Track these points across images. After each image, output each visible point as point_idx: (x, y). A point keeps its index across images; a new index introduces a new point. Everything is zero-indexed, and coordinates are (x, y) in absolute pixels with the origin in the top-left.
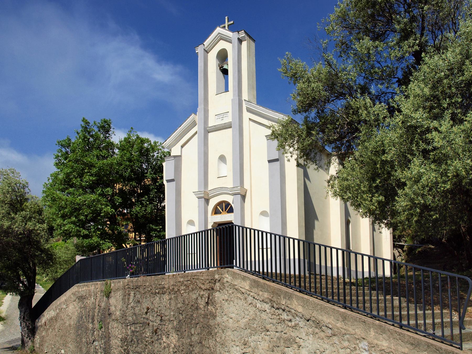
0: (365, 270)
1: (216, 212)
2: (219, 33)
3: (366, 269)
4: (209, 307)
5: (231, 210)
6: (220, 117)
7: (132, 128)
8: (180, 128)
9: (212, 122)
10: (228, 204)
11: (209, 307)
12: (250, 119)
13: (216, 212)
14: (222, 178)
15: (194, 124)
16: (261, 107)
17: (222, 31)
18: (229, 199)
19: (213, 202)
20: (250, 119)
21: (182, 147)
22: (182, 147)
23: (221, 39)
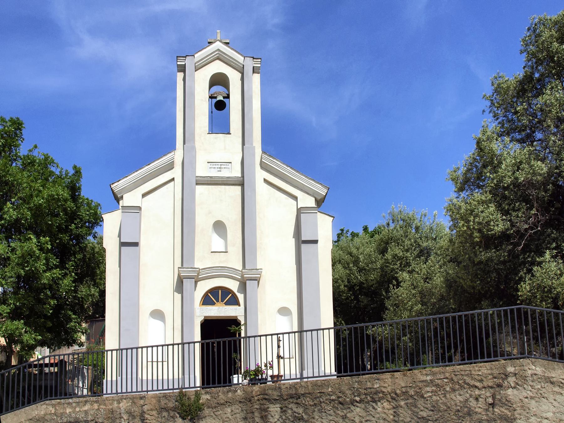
0: (164, 378)
1: (207, 300)
2: (218, 50)
3: (293, 372)
4: (495, 410)
5: (234, 301)
6: (216, 166)
7: (36, 147)
8: (147, 167)
9: (202, 170)
10: (226, 291)
11: (495, 410)
12: (265, 180)
13: (207, 300)
14: (215, 254)
15: (170, 166)
16: (289, 168)
17: (225, 49)
18: (233, 286)
19: (204, 287)
20: (265, 180)
21: (144, 195)
22: (144, 195)
23: (218, 59)
